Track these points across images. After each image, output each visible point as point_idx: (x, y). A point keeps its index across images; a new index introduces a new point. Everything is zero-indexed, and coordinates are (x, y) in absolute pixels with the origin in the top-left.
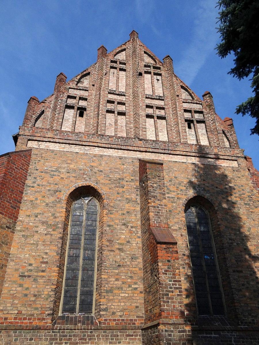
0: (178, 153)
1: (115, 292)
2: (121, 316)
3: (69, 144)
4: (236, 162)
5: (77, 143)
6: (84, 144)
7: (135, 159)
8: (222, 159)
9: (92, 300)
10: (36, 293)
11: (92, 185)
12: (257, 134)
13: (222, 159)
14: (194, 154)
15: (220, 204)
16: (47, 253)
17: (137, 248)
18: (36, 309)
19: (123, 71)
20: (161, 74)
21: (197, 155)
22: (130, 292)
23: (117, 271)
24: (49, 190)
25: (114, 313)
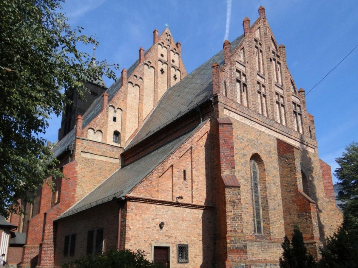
0: (292, 137)
1: (275, 223)
2: (278, 236)
3: (244, 117)
4: (313, 150)
5: (248, 117)
6: (252, 119)
7: (274, 137)
8: (310, 147)
9: (261, 226)
10: (247, 222)
11: (259, 154)
12: (136, 252)
13: (310, 147)
14: (298, 140)
15: (309, 178)
16: (247, 198)
17: (167, 217)
18: (248, 230)
19: (205, 195)
20: (266, 96)
21: (300, 141)
22: (279, 224)
23: (274, 212)
24: (241, 153)
25: (275, 235)
